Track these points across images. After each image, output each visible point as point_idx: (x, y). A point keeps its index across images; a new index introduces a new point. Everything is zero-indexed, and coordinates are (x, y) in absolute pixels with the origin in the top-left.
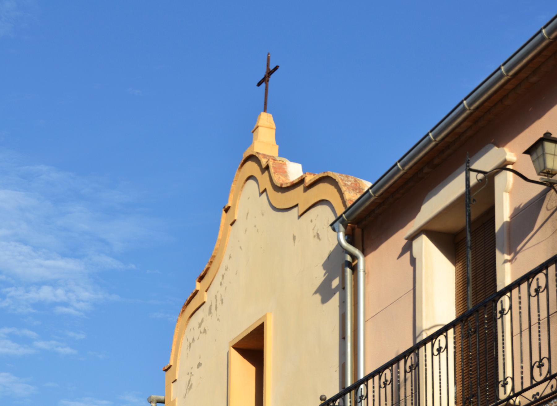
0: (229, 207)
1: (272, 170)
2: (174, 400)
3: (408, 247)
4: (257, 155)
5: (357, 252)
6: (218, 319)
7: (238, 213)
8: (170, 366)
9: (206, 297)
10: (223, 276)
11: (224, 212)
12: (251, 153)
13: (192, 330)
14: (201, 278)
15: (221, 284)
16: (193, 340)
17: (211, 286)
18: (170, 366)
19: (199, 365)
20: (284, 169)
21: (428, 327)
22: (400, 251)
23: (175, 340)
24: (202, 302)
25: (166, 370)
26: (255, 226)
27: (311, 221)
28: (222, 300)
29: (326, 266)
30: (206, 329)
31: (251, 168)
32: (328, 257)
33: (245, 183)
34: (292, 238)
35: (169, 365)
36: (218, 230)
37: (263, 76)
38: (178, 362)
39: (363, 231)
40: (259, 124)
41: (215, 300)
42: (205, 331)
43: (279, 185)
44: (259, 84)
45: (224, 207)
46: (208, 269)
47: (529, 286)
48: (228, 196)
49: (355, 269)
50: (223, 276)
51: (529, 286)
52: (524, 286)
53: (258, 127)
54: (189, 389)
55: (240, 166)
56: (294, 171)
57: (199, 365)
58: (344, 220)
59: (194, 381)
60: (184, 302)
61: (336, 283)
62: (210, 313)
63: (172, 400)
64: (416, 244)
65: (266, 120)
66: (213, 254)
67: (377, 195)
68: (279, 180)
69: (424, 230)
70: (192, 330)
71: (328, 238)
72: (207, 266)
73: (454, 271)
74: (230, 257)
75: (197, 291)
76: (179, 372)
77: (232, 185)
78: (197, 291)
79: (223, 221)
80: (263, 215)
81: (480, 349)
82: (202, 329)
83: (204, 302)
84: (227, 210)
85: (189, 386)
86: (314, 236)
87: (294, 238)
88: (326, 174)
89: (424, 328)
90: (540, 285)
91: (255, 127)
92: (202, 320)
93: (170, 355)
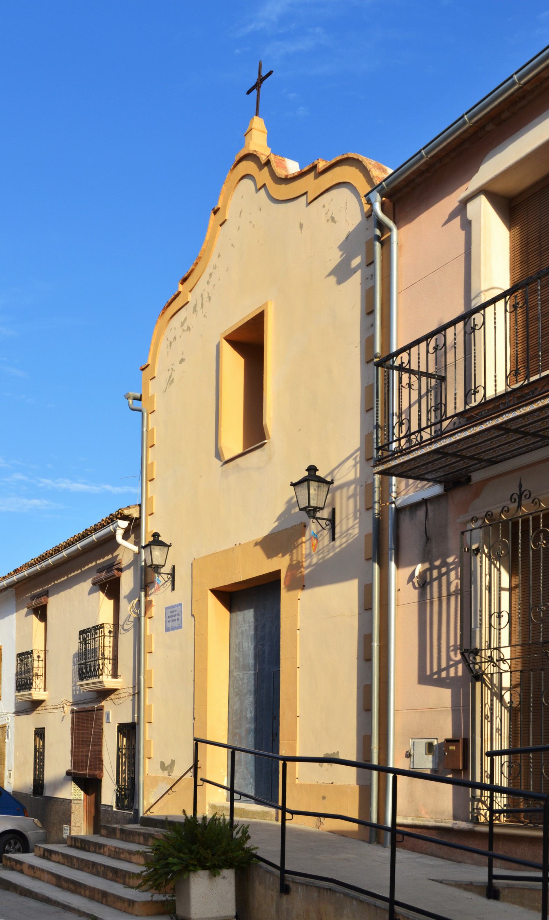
0: (219, 209)
1: (273, 164)
2: (153, 396)
3: (461, 208)
4: (255, 153)
5: (391, 224)
6: (205, 316)
7: (229, 213)
8: (148, 365)
9: (190, 297)
10: (210, 275)
11: (213, 214)
12: (246, 152)
13: (173, 329)
14: (184, 280)
15: (208, 283)
16: (175, 338)
17: (198, 282)
18: (148, 365)
19: (182, 360)
20: (284, 164)
21: (486, 289)
22: (447, 217)
23: (153, 341)
24: (186, 302)
25: (143, 370)
26: (251, 222)
27: (324, 206)
28: (209, 298)
29: (341, 247)
30: (190, 326)
31: (248, 167)
32: (347, 238)
33: (238, 183)
34: (299, 226)
35: (147, 364)
36: (206, 231)
37: (254, 83)
38: (157, 361)
39: (394, 204)
40: (253, 127)
41: (201, 299)
42: (189, 329)
43: (284, 177)
44: (249, 92)
45: (213, 209)
46: (192, 270)
47: (428, 345)
48: (218, 198)
49: (386, 244)
50: (210, 275)
51: (428, 345)
52: (423, 345)
53: (251, 129)
54: (170, 384)
55: (233, 166)
56: (293, 167)
57: (182, 360)
58: (383, 188)
59: (175, 376)
60: (165, 304)
61: (356, 261)
62: (195, 310)
63: (150, 395)
64: (470, 206)
65: (258, 123)
66: (199, 255)
67: (429, 156)
68: (280, 173)
69: (483, 191)
70: (173, 329)
71: (346, 220)
72: (191, 268)
73: (509, 236)
74: (219, 256)
75: (179, 293)
76: (159, 369)
77: (223, 187)
78: (179, 293)
79: (211, 223)
80: (260, 210)
81: (543, 311)
82: (185, 327)
83: (188, 302)
84: (215, 212)
85: (170, 381)
86: (328, 220)
87: (301, 226)
88: (345, 156)
89: (483, 288)
90: (403, 361)
91: (247, 131)
92: (185, 319)
93: (148, 355)
